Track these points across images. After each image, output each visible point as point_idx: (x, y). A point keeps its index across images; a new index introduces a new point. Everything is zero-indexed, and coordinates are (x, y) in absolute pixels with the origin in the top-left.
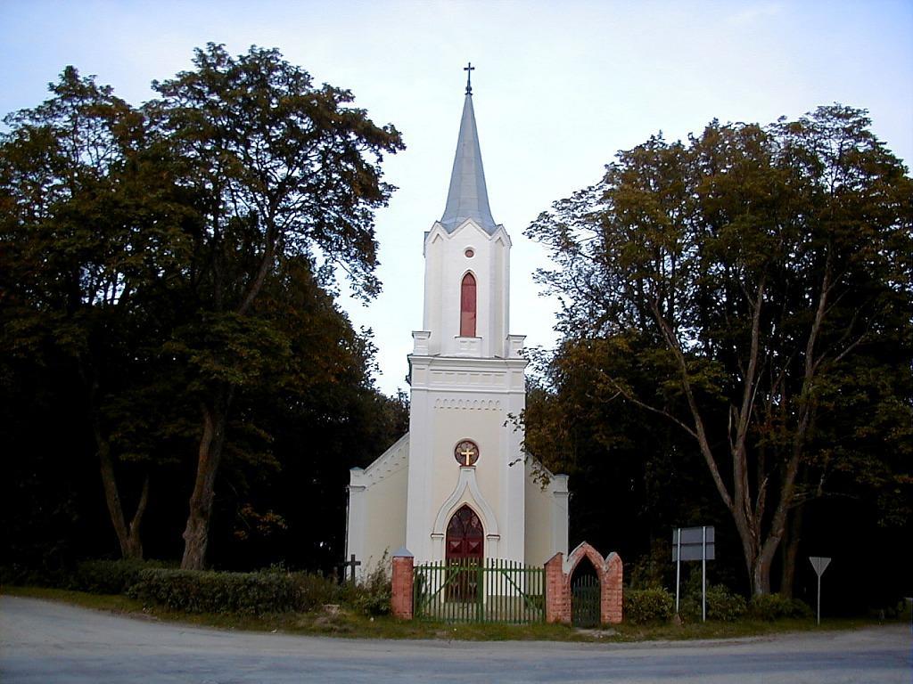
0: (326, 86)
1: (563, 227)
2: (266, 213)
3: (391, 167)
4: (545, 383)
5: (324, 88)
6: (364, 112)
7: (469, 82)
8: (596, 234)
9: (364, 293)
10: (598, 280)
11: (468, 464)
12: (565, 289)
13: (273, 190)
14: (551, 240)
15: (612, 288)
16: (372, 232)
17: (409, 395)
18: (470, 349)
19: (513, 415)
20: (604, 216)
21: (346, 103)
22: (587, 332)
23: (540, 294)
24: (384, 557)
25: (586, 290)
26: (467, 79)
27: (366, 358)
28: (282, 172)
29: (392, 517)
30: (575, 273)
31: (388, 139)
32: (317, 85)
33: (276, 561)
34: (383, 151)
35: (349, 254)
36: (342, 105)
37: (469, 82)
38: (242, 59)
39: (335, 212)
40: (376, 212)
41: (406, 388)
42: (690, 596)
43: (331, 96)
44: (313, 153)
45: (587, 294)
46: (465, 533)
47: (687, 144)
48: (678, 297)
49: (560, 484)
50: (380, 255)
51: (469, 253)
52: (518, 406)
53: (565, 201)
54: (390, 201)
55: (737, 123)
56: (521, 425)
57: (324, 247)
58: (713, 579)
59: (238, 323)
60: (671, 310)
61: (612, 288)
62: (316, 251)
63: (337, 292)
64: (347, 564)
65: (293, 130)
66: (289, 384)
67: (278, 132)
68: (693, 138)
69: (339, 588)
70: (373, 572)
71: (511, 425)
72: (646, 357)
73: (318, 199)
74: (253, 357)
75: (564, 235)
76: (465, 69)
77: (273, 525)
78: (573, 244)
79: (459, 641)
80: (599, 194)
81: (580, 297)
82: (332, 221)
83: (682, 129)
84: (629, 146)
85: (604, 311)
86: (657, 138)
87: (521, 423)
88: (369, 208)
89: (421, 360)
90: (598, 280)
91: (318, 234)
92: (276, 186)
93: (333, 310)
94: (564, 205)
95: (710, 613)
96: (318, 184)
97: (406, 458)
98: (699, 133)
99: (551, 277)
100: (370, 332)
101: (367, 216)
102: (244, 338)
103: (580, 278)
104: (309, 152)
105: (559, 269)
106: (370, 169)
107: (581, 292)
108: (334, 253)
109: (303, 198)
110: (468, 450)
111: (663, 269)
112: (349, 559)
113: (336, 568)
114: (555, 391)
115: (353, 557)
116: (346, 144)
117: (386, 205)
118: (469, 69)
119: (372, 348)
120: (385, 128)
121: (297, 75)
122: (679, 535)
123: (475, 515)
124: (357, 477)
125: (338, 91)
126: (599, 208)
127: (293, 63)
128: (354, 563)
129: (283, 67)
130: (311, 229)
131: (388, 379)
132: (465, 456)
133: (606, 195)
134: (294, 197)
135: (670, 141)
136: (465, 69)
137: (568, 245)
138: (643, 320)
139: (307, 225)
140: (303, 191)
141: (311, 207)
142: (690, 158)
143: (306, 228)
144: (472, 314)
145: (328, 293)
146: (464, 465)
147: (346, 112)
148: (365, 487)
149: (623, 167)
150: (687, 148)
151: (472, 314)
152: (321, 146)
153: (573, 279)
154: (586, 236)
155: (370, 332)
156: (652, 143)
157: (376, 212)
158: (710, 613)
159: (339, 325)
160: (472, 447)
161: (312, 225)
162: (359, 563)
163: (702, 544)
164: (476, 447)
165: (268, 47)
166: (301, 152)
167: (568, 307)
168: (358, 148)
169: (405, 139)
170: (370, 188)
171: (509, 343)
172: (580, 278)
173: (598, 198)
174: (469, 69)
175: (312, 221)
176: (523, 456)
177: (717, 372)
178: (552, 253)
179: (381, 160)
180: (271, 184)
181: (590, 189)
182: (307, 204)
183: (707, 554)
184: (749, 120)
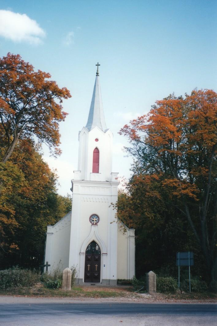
0: (40, 72)
1: (133, 131)
2: (15, 122)
3: (66, 105)
4: (126, 191)
5: (38, 72)
6: (54, 82)
7: (97, 71)
8: (146, 134)
9: (55, 155)
10: (147, 151)
11: (95, 224)
12: (134, 155)
13: (17, 113)
14: (129, 136)
15: (153, 154)
16: (58, 131)
17: (72, 195)
18: (95, 177)
19: (113, 204)
20: (149, 126)
21: (48, 78)
22: (143, 172)
23: (124, 156)
24: (60, 262)
25: (142, 155)
26: (97, 69)
27: (55, 180)
28: (21, 105)
29: (65, 246)
30: (138, 148)
31: (64, 93)
32: (36, 70)
33: (15, 265)
34: (62, 98)
35: (48, 140)
36: (46, 79)
37: (97, 71)
38: (4, 58)
39: (43, 123)
40: (59, 123)
41: (70, 193)
42: (184, 281)
43: (40, 76)
44: (34, 98)
45: (143, 157)
46: (93, 254)
47: (184, 98)
48: (180, 158)
49: (131, 233)
50: (61, 139)
51: (97, 140)
52: (115, 200)
53: (134, 121)
54: (65, 119)
55: (205, 89)
56: (116, 208)
57: (38, 137)
58: (194, 274)
59: (2, 166)
60: (176, 162)
61: (153, 154)
62: (35, 138)
63: (43, 153)
64: (45, 266)
65: (26, 88)
66: (23, 191)
67: (19, 89)
68: (187, 95)
69: (41, 276)
70: (55, 269)
71: (112, 207)
72: (165, 182)
73: (36, 117)
74: (8, 180)
75: (134, 134)
76: (96, 65)
77: (14, 249)
78: (138, 137)
79: (89, 298)
80: (148, 118)
81: (140, 158)
82: (42, 126)
83: (182, 90)
84: (161, 99)
85: (149, 163)
86: (172, 95)
87: (116, 207)
88: (57, 121)
89: (77, 182)
90: (147, 151)
91: (36, 131)
92: (19, 111)
93: (41, 161)
94: (134, 122)
95: (193, 288)
96: (36, 112)
97: (70, 221)
98: (189, 94)
99: (129, 150)
100: (56, 170)
101: (56, 125)
102: (5, 173)
103: (140, 150)
104: (32, 98)
105: (132, 146)
106: (57, 106)
107: (141, 156)
108: (42, 139)
109: (30, 117)
110: (95, 218)
111: (173, 147)
112: (45, 264)
113: (40, 268)
114: (130, 195)
115: (47, 263)
116: (47, 95)
117: (64, 121)
118: (98, 65)
119: (57, 176)
120: (63, 89)
121: (27, 66)
122: (179, 255)
123: (97, 245)
124: (50, 229)
125: (44, 73)
126: (148, 123)
127: (26, 61)
128: (48, 265)
129: (22, 63)
130: (33, 129)
131: (62, 190)
132: (94, 220)
133: (150, 119)
134: (27, 117)
135: (177, 95)
136: (99, 65)
137: (136, 139)
138: (165, 167)
139: (31, 128)
140: (30, 114)
141: (33, 120)
142: (185, 103)
143: (32, 129)
144: (97, 164)
145: (39, 154)
146: (93, 224)
147: (48, 82)
148: (53, 233)
149: (158, 107)
150: (184, 99)
151: (97, 164)
152: (37, 96)
153: (138, 151)
154: (142, 135)
155: (56, 170)
156: (170, 96)
157: (59, 123)
158: (193, 288)
159: (43, 167)
160: (96, 216)
161: (33, 128)
162: (49, 265)
163: (188, 259)
164: (98, 217)
165: (15, 54)
166: (29, 98)
167: (135, 161)
168: (53, 97)
169: (71, 93)
170: (58, 114)
171: (112, 176)
172: (140, 150)
173: (148, 119)
174: (98, 65)
175: (34, 126)
176: (116, 220)
177: (194, 189)
178: (129, 141)
179: (61, 101)
180: (17, 111)
181: (144, 116)
182: (32, 119)
183: (189, 263)
184: (210, 88)
